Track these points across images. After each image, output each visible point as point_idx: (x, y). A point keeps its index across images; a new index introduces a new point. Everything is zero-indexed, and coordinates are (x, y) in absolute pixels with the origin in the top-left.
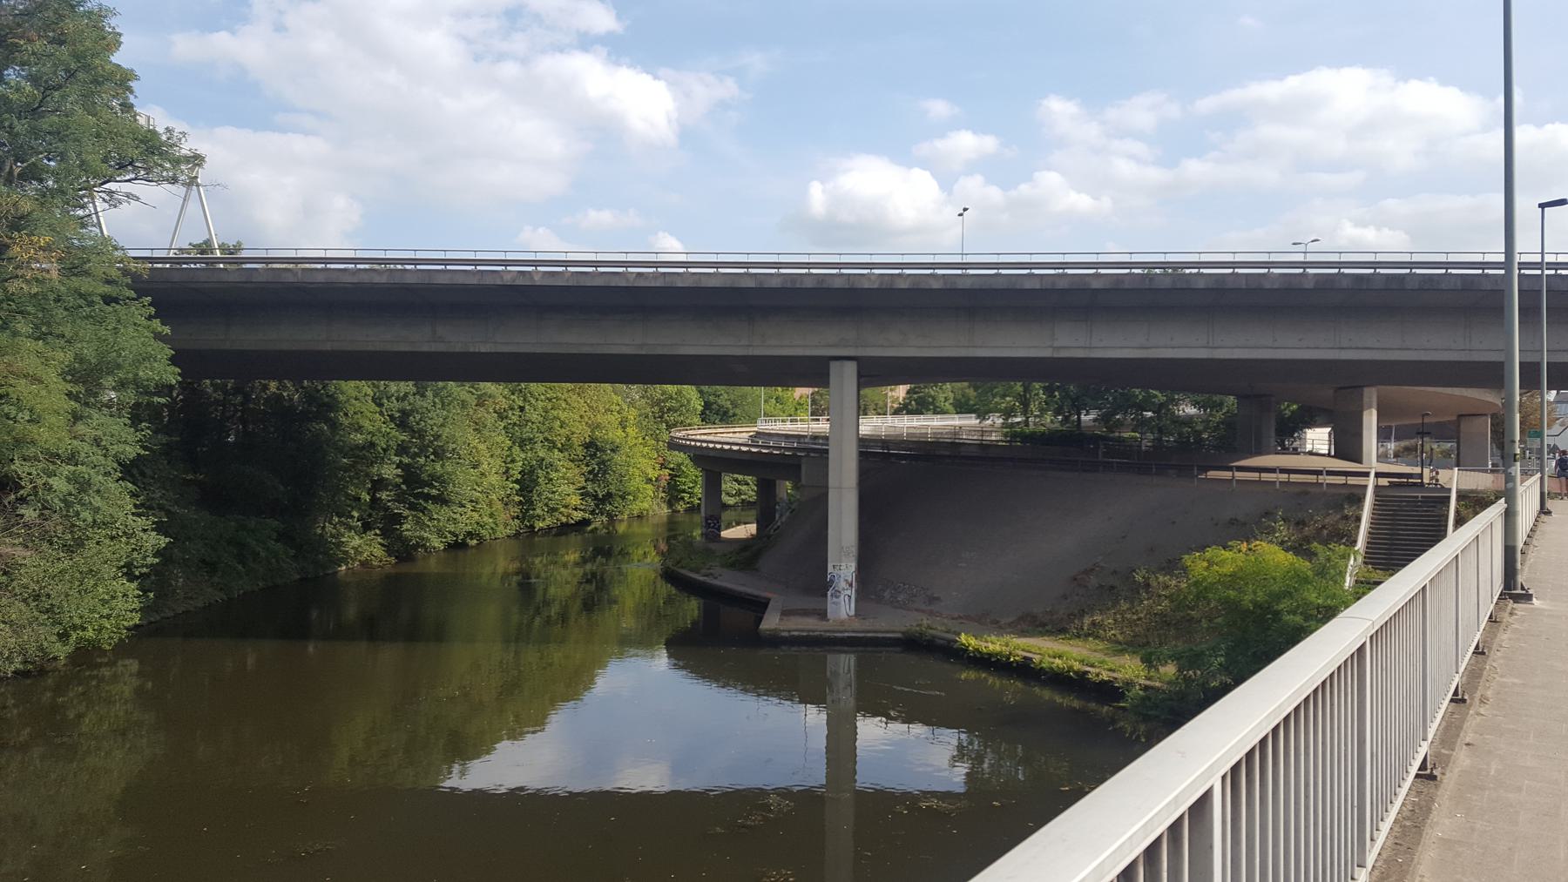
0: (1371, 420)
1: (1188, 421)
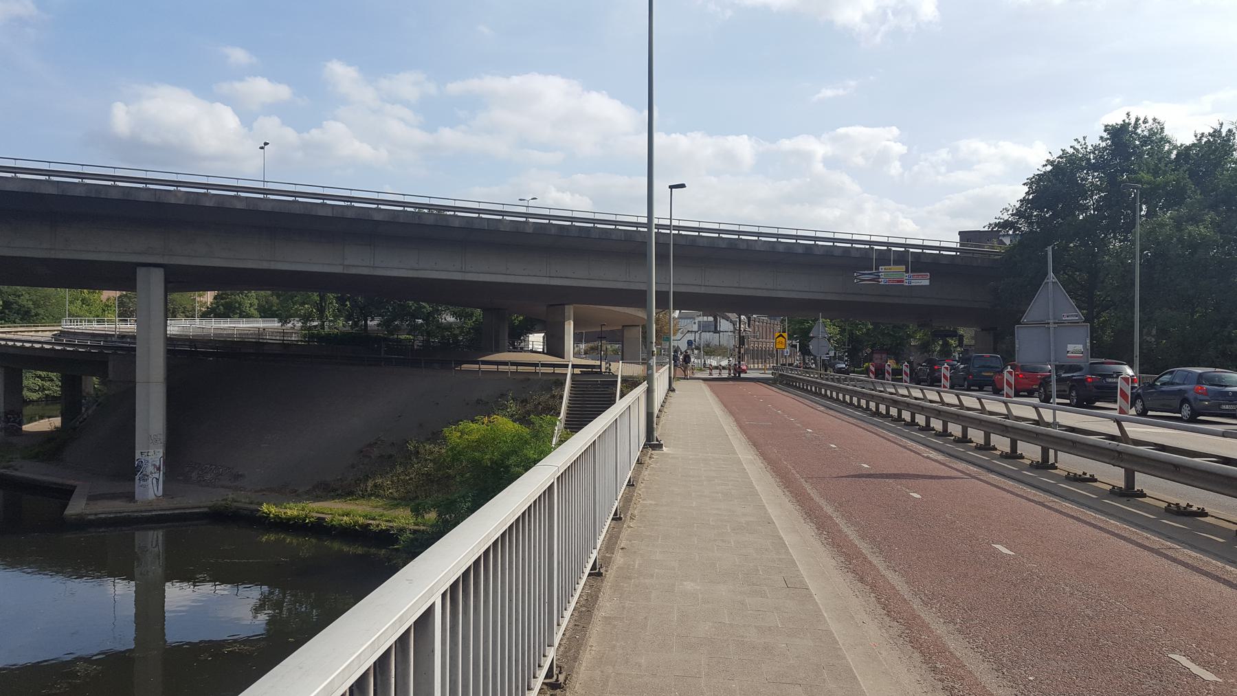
0: (570, 328)
1: (449, 326)
